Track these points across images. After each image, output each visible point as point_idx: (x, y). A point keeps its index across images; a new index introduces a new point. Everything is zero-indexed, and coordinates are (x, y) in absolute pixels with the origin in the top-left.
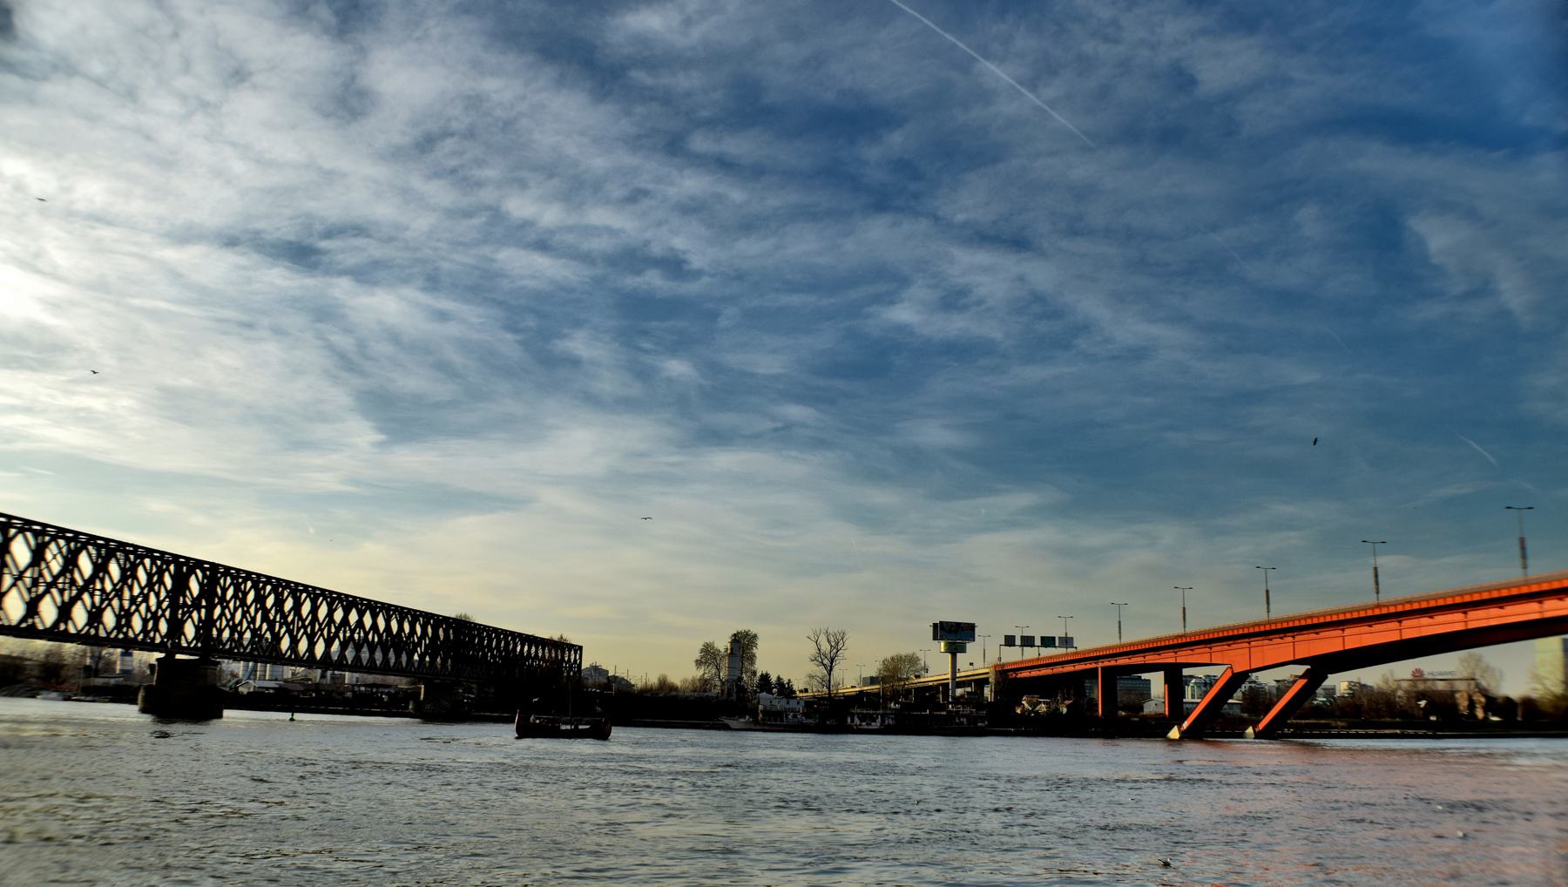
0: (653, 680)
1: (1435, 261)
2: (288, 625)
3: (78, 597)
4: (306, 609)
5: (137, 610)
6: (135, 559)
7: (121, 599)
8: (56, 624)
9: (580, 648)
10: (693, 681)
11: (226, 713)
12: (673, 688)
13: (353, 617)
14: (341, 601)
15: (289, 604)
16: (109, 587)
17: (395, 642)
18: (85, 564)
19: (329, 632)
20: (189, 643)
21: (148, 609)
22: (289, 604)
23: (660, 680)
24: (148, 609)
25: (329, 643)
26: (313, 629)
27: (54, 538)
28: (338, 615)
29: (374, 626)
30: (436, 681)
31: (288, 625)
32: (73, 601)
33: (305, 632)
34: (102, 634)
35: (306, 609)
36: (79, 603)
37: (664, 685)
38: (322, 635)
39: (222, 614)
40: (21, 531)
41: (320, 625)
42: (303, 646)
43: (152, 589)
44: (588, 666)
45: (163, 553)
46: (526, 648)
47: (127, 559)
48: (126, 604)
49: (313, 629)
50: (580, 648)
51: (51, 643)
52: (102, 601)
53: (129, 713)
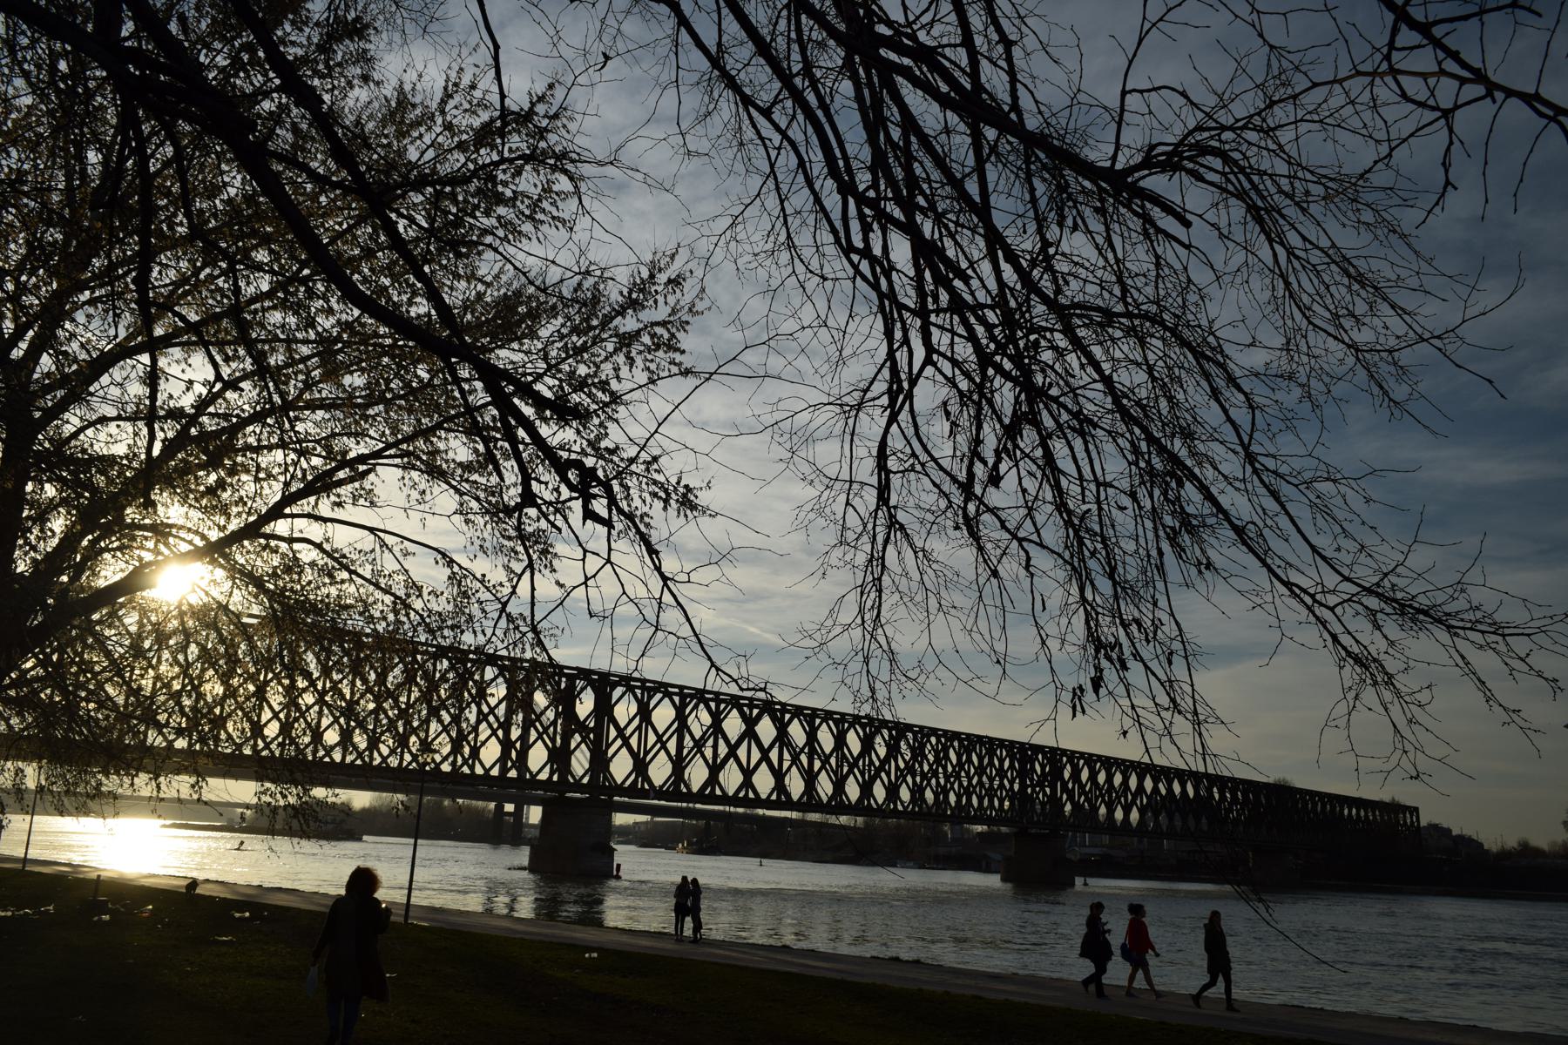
0: (1512, 843)
1: (1129, 917)
2: (1086, 794)
3: (877, 775)
4: (1102, 778)
5: (929, 784)
6: (922, 738)
7: (888, 774)
8: (860, 800)
9: (1416, 809)
10: (116, 814)
11: (1079, 881)
12: (1538, 852)
13: (1148, 784)
14: (1118, 767)
15: (1085, 775)
16: (902, 765)
17: (1202, 802)
18: (854, 742)
19: (1126, 800)
20: (487, 771)
21: (961, 785)
22: (1085, 775)
23: (1520, 845)
24: (961, 785)
25: (1142, 811)
26: (1110, 797)
27: (852, 725)
28: (1118, 779)
29: (1156, 790)
30: (563, 686)
31: (1086, 794)
32: (872, 780)
33: (1103, 801)
34: (479, 770)
35: (1102, 778)
36: (878, 780)
37: (1526, 850)
38: (1120, 802)
39: (1012, 782)
40: (825, 720)
41: (1117, 793)
42: (1119, 814)
43: (962, 768)
44: (617, 859)
45: (921, 728)
46: (1354, 811)
47: (938, 741)
48: (942, 781)
49: (1110, 797)
50: (1416, 809)
51: (386, 796)
52: (922, 782)
53: (993, 881)
